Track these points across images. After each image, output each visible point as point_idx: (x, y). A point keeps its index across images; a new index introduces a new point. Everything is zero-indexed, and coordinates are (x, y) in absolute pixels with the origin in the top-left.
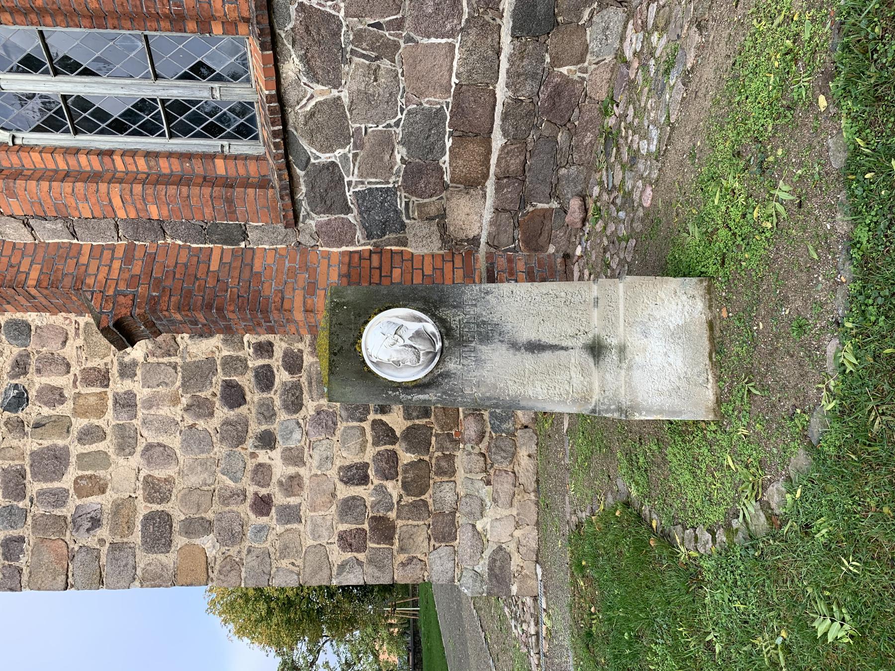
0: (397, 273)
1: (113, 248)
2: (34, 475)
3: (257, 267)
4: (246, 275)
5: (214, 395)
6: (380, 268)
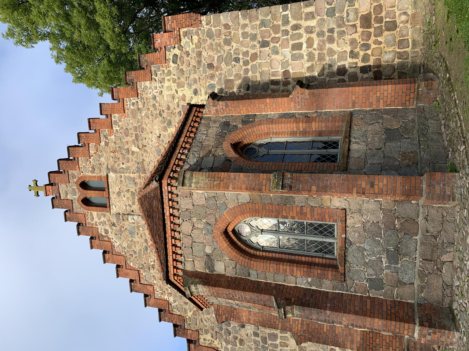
0: (378, 340)
1: (298, 320)
2: (269, 339)
3: (337, 333)
4: (334, 335)
5: (270, 48)
6: (372, 338)
